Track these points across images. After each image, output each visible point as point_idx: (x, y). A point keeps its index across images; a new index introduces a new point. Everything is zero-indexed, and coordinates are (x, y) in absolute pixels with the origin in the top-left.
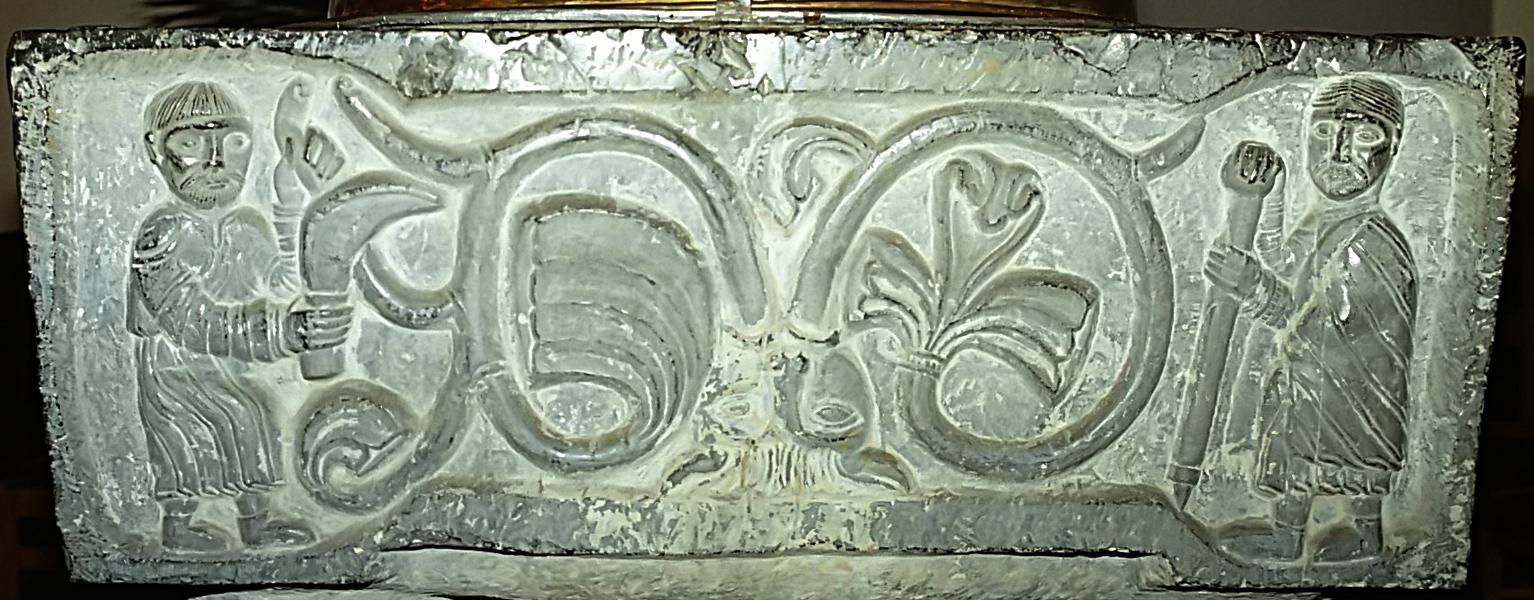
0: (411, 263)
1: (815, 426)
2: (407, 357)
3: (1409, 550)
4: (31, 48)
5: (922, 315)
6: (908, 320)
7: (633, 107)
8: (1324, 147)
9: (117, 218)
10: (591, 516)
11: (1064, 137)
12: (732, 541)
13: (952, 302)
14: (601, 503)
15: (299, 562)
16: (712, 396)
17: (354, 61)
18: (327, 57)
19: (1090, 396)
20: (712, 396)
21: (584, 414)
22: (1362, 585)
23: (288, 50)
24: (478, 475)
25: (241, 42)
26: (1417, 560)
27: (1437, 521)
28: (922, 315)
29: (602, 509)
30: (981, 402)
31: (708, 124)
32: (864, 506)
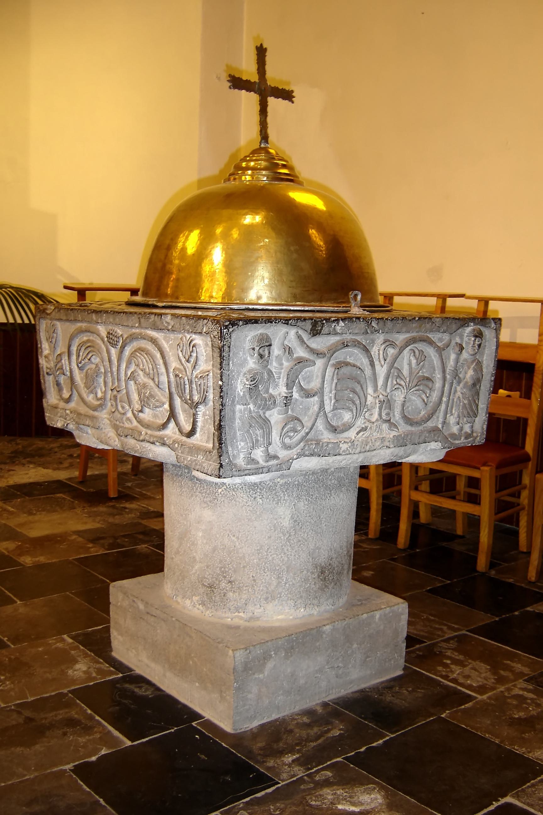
0: (304, 381)
1: (384, 418)
2: (301, 407)
3: (477, 437)
4: (229, 324)
5: (405, 388)
6: (402, 389)
7: (193, 305)
8: (469, 343)
9: (237, 372)
10: (341, 445)
11: (431, 343)
12: (368, 448)
13: (410, 385)
14: (343, 442)
15: (277, 465)
16: (366, 412)
17: (302, 327)
18: (295, 326)
19: (135, 600)
20: (366, 412)
21: (337, 419)
22: (470, 445)
23: (287, 324)
24: (315, 438)
25: (277, 322)
26: (478, 438)
27: (488, 391)
28: (405, 388)
29: (343, 443)
30: (410, 408)
31: (367, 341)
32: (391, 436)
